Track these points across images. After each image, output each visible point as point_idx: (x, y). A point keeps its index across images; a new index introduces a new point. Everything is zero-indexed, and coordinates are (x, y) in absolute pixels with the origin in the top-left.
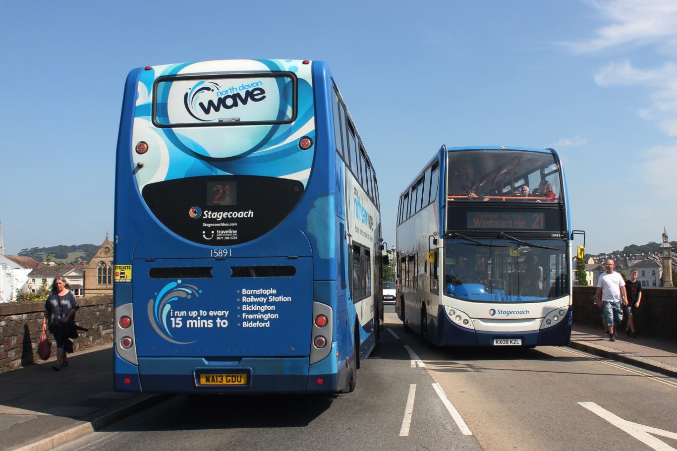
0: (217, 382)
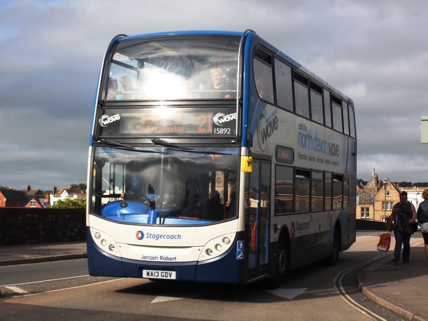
0: (155, 276)
